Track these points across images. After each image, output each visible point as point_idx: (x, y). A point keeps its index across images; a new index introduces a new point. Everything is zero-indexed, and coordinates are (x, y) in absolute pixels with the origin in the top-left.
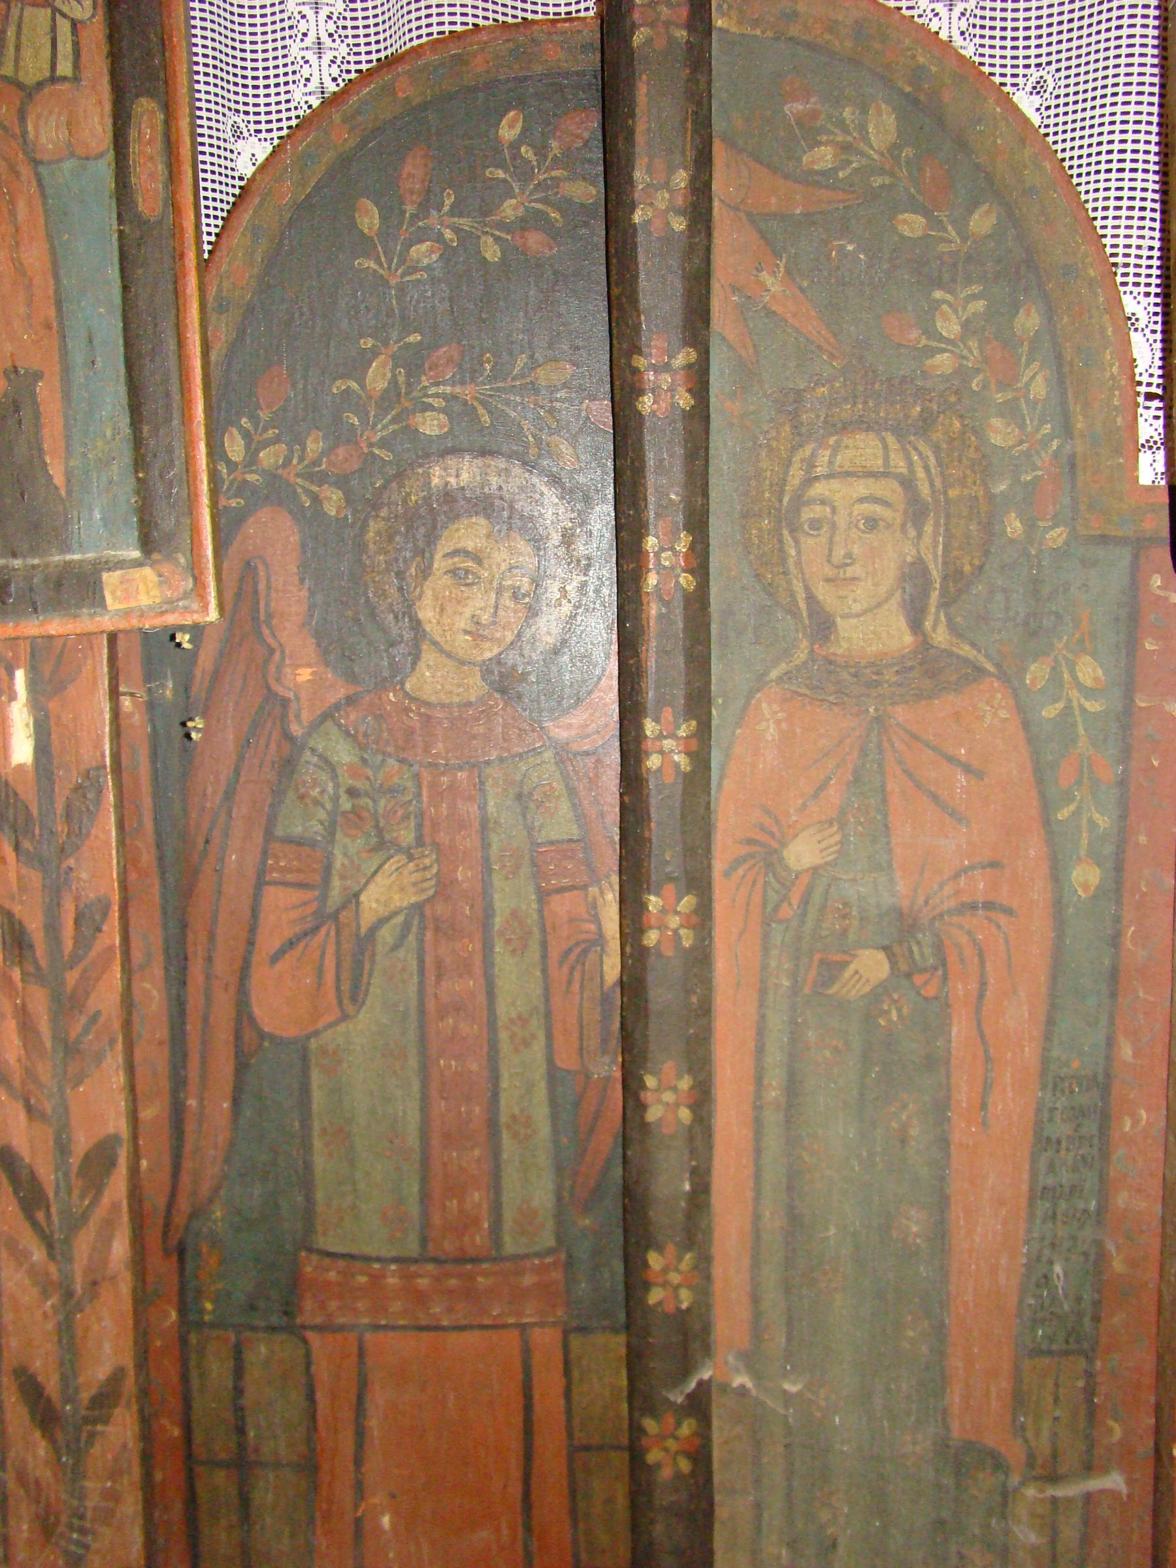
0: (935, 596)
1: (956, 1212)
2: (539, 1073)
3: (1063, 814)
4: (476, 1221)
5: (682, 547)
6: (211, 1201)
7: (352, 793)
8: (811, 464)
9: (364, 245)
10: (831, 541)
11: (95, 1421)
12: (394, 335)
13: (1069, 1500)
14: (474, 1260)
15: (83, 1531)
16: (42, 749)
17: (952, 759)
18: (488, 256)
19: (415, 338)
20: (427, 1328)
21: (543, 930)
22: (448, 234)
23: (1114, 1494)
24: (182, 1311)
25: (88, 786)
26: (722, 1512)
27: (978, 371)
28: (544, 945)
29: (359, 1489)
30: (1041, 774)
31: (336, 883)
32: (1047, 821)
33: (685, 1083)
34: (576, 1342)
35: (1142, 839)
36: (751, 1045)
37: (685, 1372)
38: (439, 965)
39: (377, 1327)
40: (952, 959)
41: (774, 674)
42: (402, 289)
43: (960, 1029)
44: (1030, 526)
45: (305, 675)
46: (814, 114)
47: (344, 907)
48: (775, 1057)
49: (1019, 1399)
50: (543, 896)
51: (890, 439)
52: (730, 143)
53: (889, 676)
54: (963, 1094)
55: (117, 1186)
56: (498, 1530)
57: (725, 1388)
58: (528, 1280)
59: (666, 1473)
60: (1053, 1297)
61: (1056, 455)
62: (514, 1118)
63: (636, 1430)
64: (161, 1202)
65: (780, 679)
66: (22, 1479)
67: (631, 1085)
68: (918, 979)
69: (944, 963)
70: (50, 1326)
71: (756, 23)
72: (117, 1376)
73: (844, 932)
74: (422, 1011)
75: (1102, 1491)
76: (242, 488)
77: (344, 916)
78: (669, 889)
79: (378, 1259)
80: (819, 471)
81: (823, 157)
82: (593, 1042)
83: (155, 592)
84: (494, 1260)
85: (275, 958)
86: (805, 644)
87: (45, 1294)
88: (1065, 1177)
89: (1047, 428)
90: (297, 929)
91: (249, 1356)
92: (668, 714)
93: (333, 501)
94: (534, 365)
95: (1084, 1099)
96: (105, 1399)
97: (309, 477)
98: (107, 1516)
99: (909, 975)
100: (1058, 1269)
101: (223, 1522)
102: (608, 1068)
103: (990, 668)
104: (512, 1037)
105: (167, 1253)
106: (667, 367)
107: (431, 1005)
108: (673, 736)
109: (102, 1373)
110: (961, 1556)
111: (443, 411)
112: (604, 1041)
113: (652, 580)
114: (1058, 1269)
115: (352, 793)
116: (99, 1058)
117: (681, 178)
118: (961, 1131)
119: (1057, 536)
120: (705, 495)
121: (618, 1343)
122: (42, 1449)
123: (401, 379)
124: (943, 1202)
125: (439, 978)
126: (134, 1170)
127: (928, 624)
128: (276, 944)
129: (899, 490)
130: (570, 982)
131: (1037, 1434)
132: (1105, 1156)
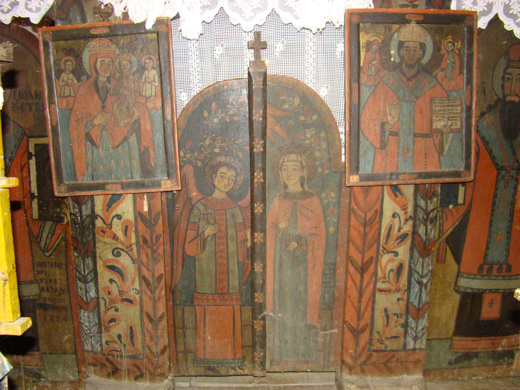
0: (306, 182)
1: (309, 286)
2: (236, 262)
3: (328, 219)
4: (225, 287)
5: (261, 175)
6: (178, 283)
7: (203, 214)
8: (284, 159)
9: (205, 119)
10: (288, 173)
11: (159, 321)
12: (210, 135)
13: (328, 334)
14: (225, 294)
15: (158, 339)
16: (149, 209)
17: (308, 209)
18: (227, 121)
19: (214, 135)
20: (217, 305)
21: (237, 238)
22: (220, 117)
23: (335, 333)
24: (173, 302)
25: (157, 216)
26: (268, 336)
27: (314, 143)
28: (237, 240)
29: (205, 333)
30: (324, 211)
31: (200, 230)
32: (325, 220)
33: (261, 265)
34: (242, 308)
35: (342, 223)
36: (273, 258)
37: (261, 312)
38: (218, 243)
39: (207, 305)
40: (308, 244)
41: (277, 195)
42: (212, 126)
43: (309, 255)
44: (323, 170)
45: (194, 194)
46: (285, 99)
47: (202, 234)
48: (277, 260)
49: (319, 317)
50: (237, 232)
51: (299, 156)
52: (269, 103)
53: (297, 195)
54: (310, 266)
55: (163, 283)
56: (229, 339)
57: (268, 315)
58: (234, 297)
59: (258, 330)
60: (326, 300)
61: (327, 157)
62: (232, 270)
63: (253, 323)
64: (169, 284)
65: (278, 196)
66: (147, 331)
67: (252, 265)
68: (302, 247)
69: (307, 244)
70: (152, 305)
71: (274, 83)
72: (163, 314)
73: (289, 239)
74: (215, 252)
75: (334, 332)
76: (183, 161)
77: (202, 235)
78: (259, 232)
79: (208, 294)
80: (286, 160)
81: (286, 106)
82: (245, 257)
83: (170, 185)
84: (228, 294)
85: (189, 243)
86: (283, 190)
87: (151, 300)
88: (328, 280)
89: (326, 153)
90: (193, 237)
91: (185, 310)
92: (258, 203)
93: (199, 164)
94: (235, 140)
95: (331, 267)
96: (161, 318)
97: (195, 159)
98: (162, 337)
99: (301, 246)
100: (326, 296)
101: (181, 338)
102: (248, 262)
103: (315, 194)
104: (231, 256)
105: (170, 293)
106: (259, 144)
107: (217, 251)
108: (260, 207)
109: (161, 313)
110: (309, 343)
111: (219, 148)
112: (247, 257)
113: (256, 180)
114: (326, 296)
115: (203, 214)
116: (160, 260)
117: (261, 111)
118: (309, 272)
119: (327, 172)
120: (265, 165)
121: (250, 308)
122: (151, 325)
123: (212, 142)
124: (306, 284)
125: (218, 246)
126: (165, 279)
127: (305, 186)
128: (189, 241)
129: (300, 164)
130: (241, 247)
131: (323, 323)
132: (335, 276)
